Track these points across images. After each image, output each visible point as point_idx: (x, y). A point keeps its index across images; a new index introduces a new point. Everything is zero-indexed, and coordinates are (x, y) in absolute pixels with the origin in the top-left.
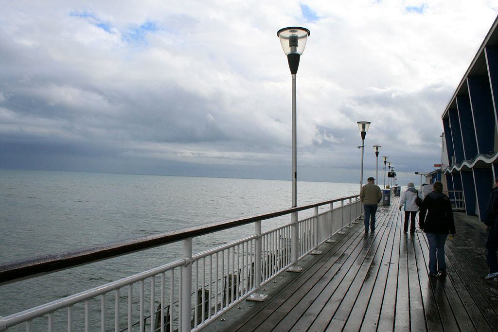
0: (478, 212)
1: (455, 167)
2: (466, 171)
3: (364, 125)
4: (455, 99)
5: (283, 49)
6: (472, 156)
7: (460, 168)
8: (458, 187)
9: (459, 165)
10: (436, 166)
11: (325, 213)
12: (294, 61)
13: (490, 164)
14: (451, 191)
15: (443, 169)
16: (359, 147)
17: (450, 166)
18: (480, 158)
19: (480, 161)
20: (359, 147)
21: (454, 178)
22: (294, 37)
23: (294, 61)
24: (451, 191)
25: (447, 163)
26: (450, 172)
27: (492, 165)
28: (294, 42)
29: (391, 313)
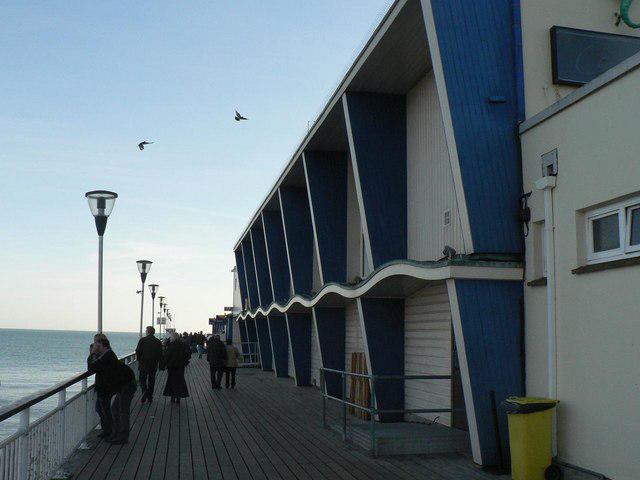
0: (274, 368)
1: (249, 313)
2: (298, 313)
3: (144, 264)
4: (277, 191)
5: (87, 213)
6: (266, 304)
7: (268, 312)
8: (253, 339)
9: (253, 313)
10: (226, 309)
11: (632, 230)
12: (101, 223)
13: (310, 308)
14: (398, 411)
15: (236, 313)
16: (138, 292)
17: (244, 313)
18: (274, 305)
19: (331, 295)
20: (138, 292)
21: (248, 326)
22: (102, 199)
23: (101, 223)
24: (398, 411)
25: (239, 304)
26: (244, 318)
27: (509, 273)
28: (101, 204)
29: (150, 464)
